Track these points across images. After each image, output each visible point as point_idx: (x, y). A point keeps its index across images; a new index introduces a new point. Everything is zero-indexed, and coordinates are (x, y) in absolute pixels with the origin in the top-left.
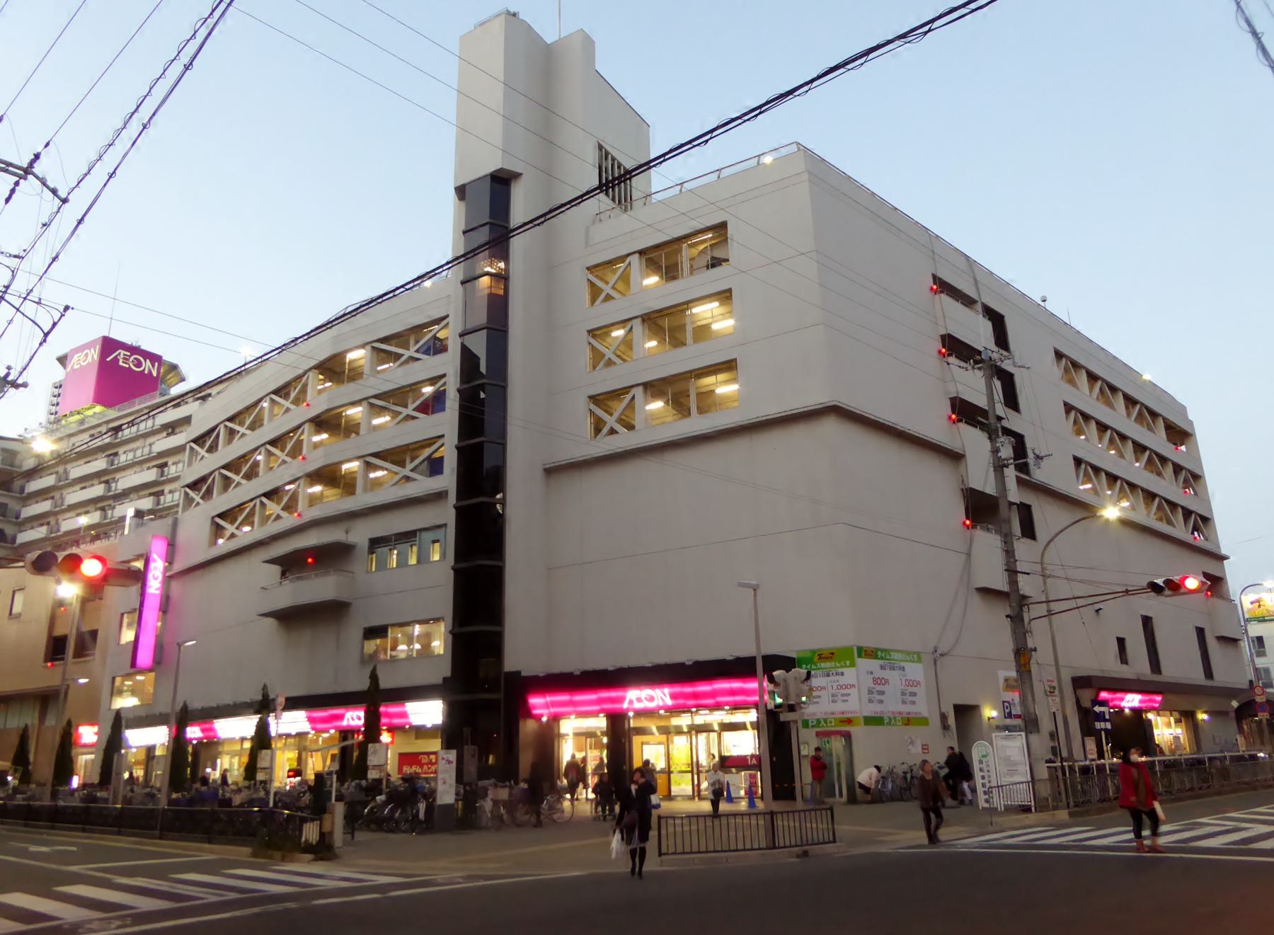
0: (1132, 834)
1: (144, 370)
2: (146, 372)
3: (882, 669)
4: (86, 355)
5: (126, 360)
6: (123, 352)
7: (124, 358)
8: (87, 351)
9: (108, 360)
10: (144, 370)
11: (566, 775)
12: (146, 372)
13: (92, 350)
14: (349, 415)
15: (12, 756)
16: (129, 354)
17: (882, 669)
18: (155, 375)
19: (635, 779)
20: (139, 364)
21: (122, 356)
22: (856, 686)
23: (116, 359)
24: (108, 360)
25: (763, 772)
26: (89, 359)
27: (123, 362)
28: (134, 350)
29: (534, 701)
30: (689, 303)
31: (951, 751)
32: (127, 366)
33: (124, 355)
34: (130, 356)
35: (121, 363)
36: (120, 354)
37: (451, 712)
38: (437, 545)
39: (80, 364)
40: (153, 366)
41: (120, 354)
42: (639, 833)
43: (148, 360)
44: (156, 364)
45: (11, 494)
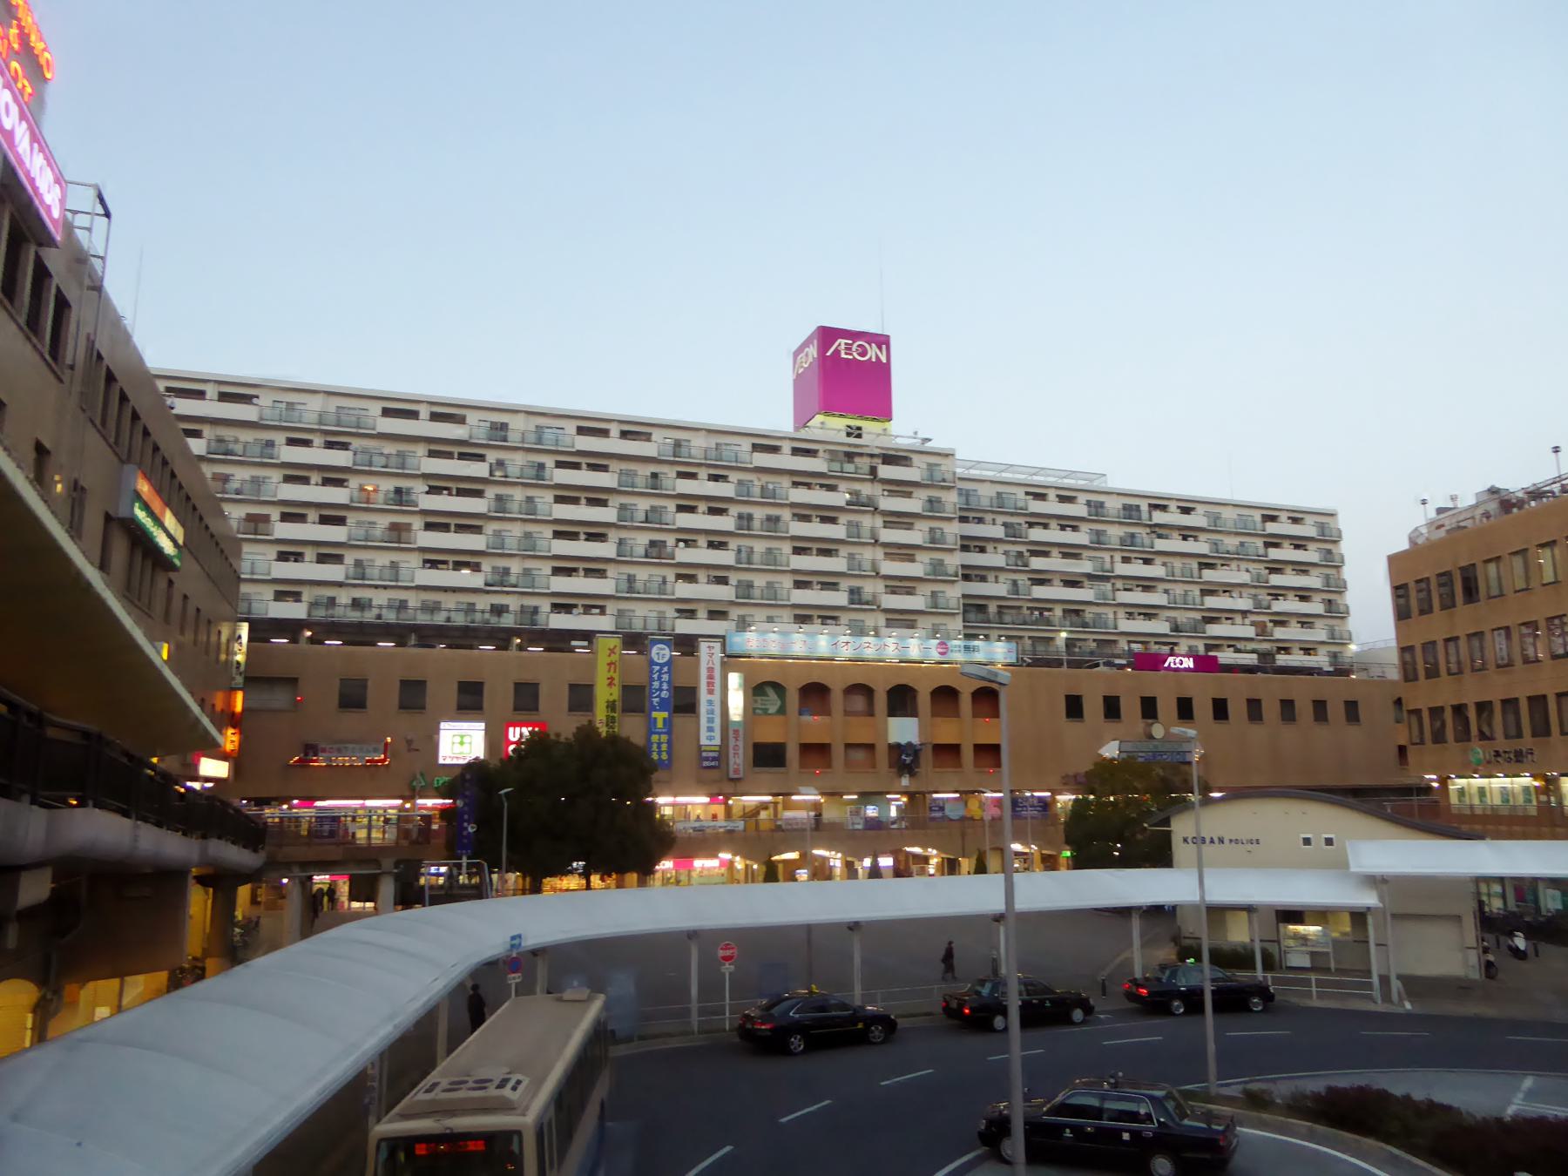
1: (871, 358)
3: (405, 684)
4: (807, 355)
5: (848, 349)
6: (843, 341)
7: (846, 348)
8: (807, 349)
9: (828, 354)
10: (871, 358)
12: (874, 360)
14: (656, 803)
15: (1546, 738)
16: (850, 342)
17: (405, 684)
18: (885, 361)
21: (843, 346)
22: (1389, 918)
23: (837, 352)
24: (828, 354)
27: (846, 354)
29: (604, 735)
30: (112, 1015)
32: (851, 357)
33: (846, 344)
35: (843, 356)
36: (840, 345)
38: (1549, 576)
39: (802, 367)
40: (877, 357)
41: (840, 345)
42: (913, 846)
43: (873, 345)
45: (751, 532)
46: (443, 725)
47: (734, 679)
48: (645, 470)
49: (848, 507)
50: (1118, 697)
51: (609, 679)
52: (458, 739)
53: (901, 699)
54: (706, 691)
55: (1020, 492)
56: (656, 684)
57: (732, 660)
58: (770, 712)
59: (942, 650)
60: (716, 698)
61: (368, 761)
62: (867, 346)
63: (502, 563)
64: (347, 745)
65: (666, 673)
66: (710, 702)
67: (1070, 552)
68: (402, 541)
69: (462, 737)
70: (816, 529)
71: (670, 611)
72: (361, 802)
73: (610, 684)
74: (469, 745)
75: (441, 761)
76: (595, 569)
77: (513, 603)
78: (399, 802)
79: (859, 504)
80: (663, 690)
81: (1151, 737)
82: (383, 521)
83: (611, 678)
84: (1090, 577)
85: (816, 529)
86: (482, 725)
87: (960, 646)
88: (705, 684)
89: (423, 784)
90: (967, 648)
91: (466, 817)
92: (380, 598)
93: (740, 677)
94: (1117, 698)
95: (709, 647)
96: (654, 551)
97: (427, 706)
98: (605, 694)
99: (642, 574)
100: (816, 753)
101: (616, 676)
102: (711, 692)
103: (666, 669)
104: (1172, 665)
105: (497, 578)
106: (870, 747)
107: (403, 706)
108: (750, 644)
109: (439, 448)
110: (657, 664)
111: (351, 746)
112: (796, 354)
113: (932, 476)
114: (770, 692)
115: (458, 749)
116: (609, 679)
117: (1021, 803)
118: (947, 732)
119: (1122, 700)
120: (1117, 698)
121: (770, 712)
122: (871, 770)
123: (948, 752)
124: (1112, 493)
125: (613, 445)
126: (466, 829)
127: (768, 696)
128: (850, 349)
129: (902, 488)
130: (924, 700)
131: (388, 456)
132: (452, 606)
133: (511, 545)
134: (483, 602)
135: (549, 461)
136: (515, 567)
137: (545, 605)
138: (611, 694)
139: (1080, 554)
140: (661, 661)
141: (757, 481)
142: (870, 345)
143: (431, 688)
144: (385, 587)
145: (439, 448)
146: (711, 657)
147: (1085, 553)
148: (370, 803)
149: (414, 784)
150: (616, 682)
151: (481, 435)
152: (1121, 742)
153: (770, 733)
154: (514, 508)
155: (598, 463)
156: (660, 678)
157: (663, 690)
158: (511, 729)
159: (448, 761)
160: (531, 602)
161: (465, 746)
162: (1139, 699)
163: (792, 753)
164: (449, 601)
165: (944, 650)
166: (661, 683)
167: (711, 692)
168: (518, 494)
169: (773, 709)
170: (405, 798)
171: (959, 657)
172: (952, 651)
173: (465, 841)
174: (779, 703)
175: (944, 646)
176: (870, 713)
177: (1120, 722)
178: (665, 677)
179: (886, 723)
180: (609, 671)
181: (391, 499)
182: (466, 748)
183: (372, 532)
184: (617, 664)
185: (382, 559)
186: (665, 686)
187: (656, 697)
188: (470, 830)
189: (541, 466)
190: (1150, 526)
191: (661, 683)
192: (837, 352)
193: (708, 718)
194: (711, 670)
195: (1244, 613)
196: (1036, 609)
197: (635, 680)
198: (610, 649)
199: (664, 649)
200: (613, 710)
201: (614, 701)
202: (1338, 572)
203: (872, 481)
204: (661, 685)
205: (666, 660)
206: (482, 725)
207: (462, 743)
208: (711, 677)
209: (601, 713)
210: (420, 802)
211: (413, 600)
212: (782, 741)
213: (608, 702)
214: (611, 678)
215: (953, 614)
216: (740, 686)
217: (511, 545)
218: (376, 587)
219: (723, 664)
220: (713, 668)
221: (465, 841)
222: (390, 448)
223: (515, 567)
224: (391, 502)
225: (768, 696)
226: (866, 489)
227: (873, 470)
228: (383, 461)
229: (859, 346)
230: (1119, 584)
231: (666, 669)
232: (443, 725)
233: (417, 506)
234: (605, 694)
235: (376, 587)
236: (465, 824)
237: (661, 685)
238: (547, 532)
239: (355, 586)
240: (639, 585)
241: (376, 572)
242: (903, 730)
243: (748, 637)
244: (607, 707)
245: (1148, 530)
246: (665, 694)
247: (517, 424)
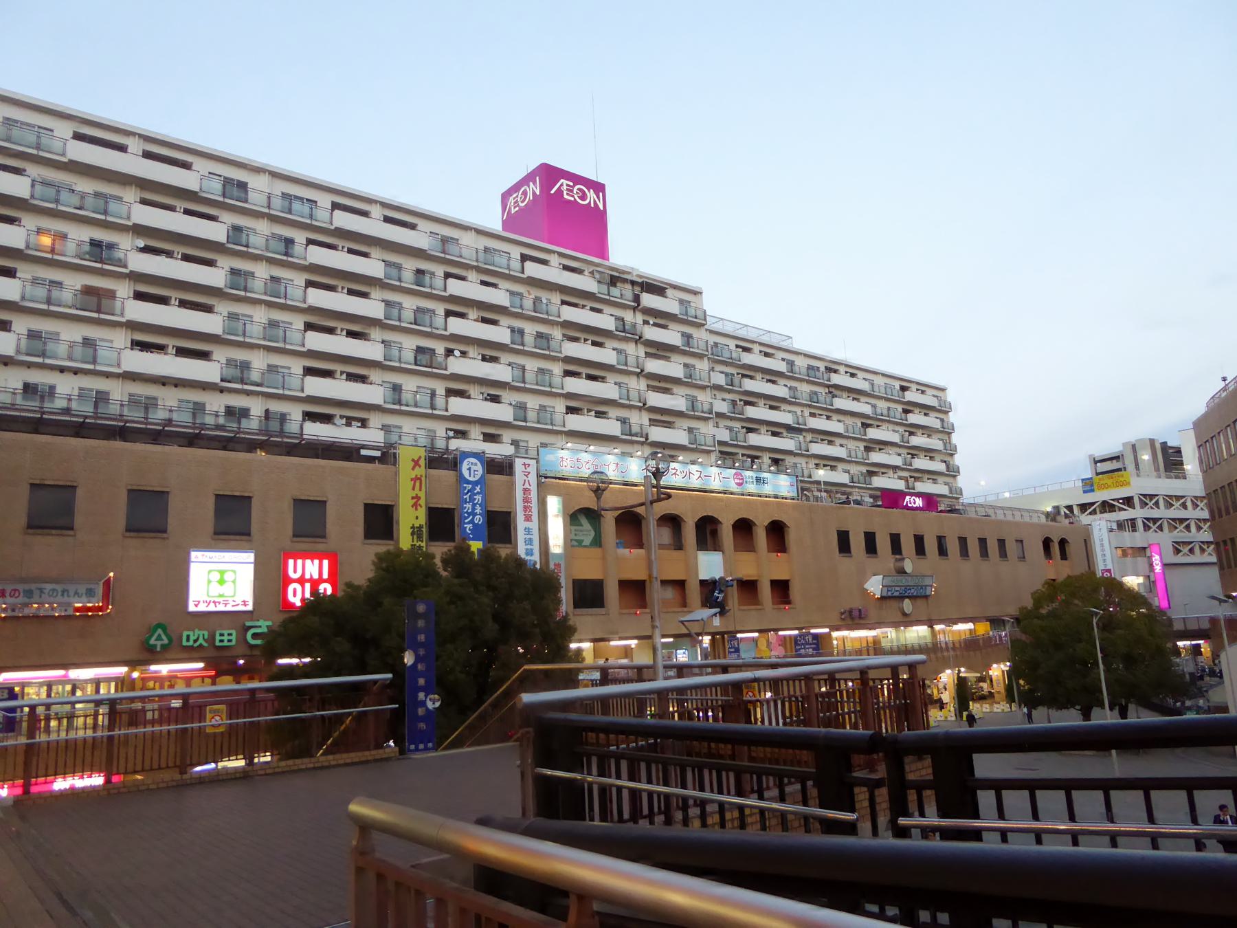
0: (911, 777)
1: (590, 202)
2: (592, 205)
4: (525, 193)
6: (565, 182)
9: (552, 192)
11: (315, 658)
13: (531, 185)
16: (571, 184)
18: (602, 208)
19: (678, 651)
20: (583, 197)
23: (559, 191)
25: (738, 629)
26: (530, 196)
28: (576, 179)
31: (619, 545)
33: (567, 185)
34: (573, 187)
36: (562, 185)
37: (300, 558)
41: (562, 185)
43: (592, 190)
44: (601, 194)
45: (103, 316)
46: (194, 555)
47: (554, 504)
48: (410, 265)
49: (617, 333)
50: (848, 531)
51: (413, 498)
52: (215, 576)
53: (708, 531)
54: (523, 518)
55: (732, 344)
56: (468, 506)
57: (547, 482)
58: (584, 544)
59: (738, 481)
60: (534, 525)
61: (77, 610)
62: (586, 190)
63: (240, 355)
64: (43, 586)
65: (478, 493)
66: (528, 530)
67: (774, 403)
68: (102, 310)
69: (222, 572)
70: (583, 351)
71: (440, 429)
72: (61, 673)
73: (415, 506)
74: (232, 584)
75: (192, 608)
76: (358, 371)
77: (256, 408)
78: (122, 670)
79: (626, 333)
80: (476, 514)
81: (901, 572)
82: (75, 282)
83: (417, 498)
84: (789, 428)
85: (583, 351)
86: (250, 557)
87: (752, 477)
88: (522, 508)
89: (166, 641)
90: (758, 480)
91: (421, 681)
92: (66, 386)
93: (559, 501)
94: (874, 534)
95: (524, 464)
96: (424, 358)
97: (170, 528)
98: (410, 518)
99: (410, 384)
100: (635, 590)
101: (422, 494)
102: (528, 518)
103: (478, 489)
104: (909, 505)
105: (237, 373)
106: (680, 585)
107: (133, 528)
108: (565, 464)
109: (153, 192)
110: (468, 482)
111: (48, 587)
112: (505, 196)
113: (687, 311)
114: (584, 520)
115: (216, 590)
116: (413, 498)
117: (800, 641)
118: (747, 567)
119: (850, 533)
120: (874, 534)
121: (584, 544)
122: (680, 609)
123: (748, 587)
124: (801, 354)
125: (374, 227)
126: (423, 703)
127: (581, 525)
128: (572, 191)
129: (662, 318)
130: (727, 534)
131: (83, 196)
132: (173, 403)
133: (255, 332)
134: (216, 404)
135: (300, 237)
136: (259, 362)
137: (295, 413)
138: (417, 518)
139: (780, 407)
140: (472, 479)
141: (530, 295)
142: (589, 191)
143: (174, 504)
144: (76, 372)
145: (153, 192)
146: (526, 476)
147: (783, 406)
148: (76, 674)
149: (152, 642)
150: (422, 502)
151: (214, 189)
152: (884, 576)
153: (590, 572)
154: (258, 287)
155: (360, 244)
156: (472, 499)
157: (476, 514)
158: (291, 562)
159: (202, 608)
160: (277, 407)
161: (226, 585)
162: (889, 536)
163: (612, 592)
164: (169, 398)
165: (741, 481)
166: (474, 505)
167: (528, 518)
168: (262, 271)
169: (587, 540)
170: (133, 664)
171: (752, 488)
172: (746, 482)
173: (422, 726)
174: (593, 533)
175: (740, 477)
176: (678, 545)
177: (876, 557)
178: (478, 498)
179: (696, 558)
180: (414, 489)
181: (87, 253)
182: (227, 590)
183: (55, 293)
184: (423, 479)
185: (71, 333)
186: (478, 510)
187: (468, 523)
188: (430, 705)
189: (289, 242)
190: (828, 386)
191: (474, 505)
192: (559, 191)
193: (527, 549)
194: (526, 491)
195: (895, 468)
196: (749, 456)
197: (444, 501)
198: (413, 460)
199: (476, 464)
200: (420, 538)
201: (421, 527)
202: (949, 438)
203: (634, 309)
204: (474, 509)
205: (477, 478)
206: (250, 557)
207: (222, 582)
208: (526, 500)
209: (405, 541)
210: (153, 668)
211: (118, 392)
212: (600, 578)
213: (413, 527)
214: (417, 498)
215: (709, 452)
216: (559, 512)
217: (255, 332)
218: (62, 370)
219: (539, 484)
220: (529, 489)
221: (422, 726)
222: (85, 186)
223: (259, 362)
224: (87, 257)
225: (581, 525)
226: (628, 316)
227: (637, 299)
228: (75, 200)
229: (579, 189)
230: (809, 437)
231: (478, 489)
232: (194, 555)
233: (125, 266)
234: (410, 518)
235: (62, 370)
236: (421, 695)
237: (474, 509)
238: (298, 322)
239: (29, 365)
240: (407, 397)
241: (62, 349)
242: (710, 565)
243: (561, 455)
244: (413, 534)
245: (827, 390)
246: (478, 519)
247: (258, 184)
